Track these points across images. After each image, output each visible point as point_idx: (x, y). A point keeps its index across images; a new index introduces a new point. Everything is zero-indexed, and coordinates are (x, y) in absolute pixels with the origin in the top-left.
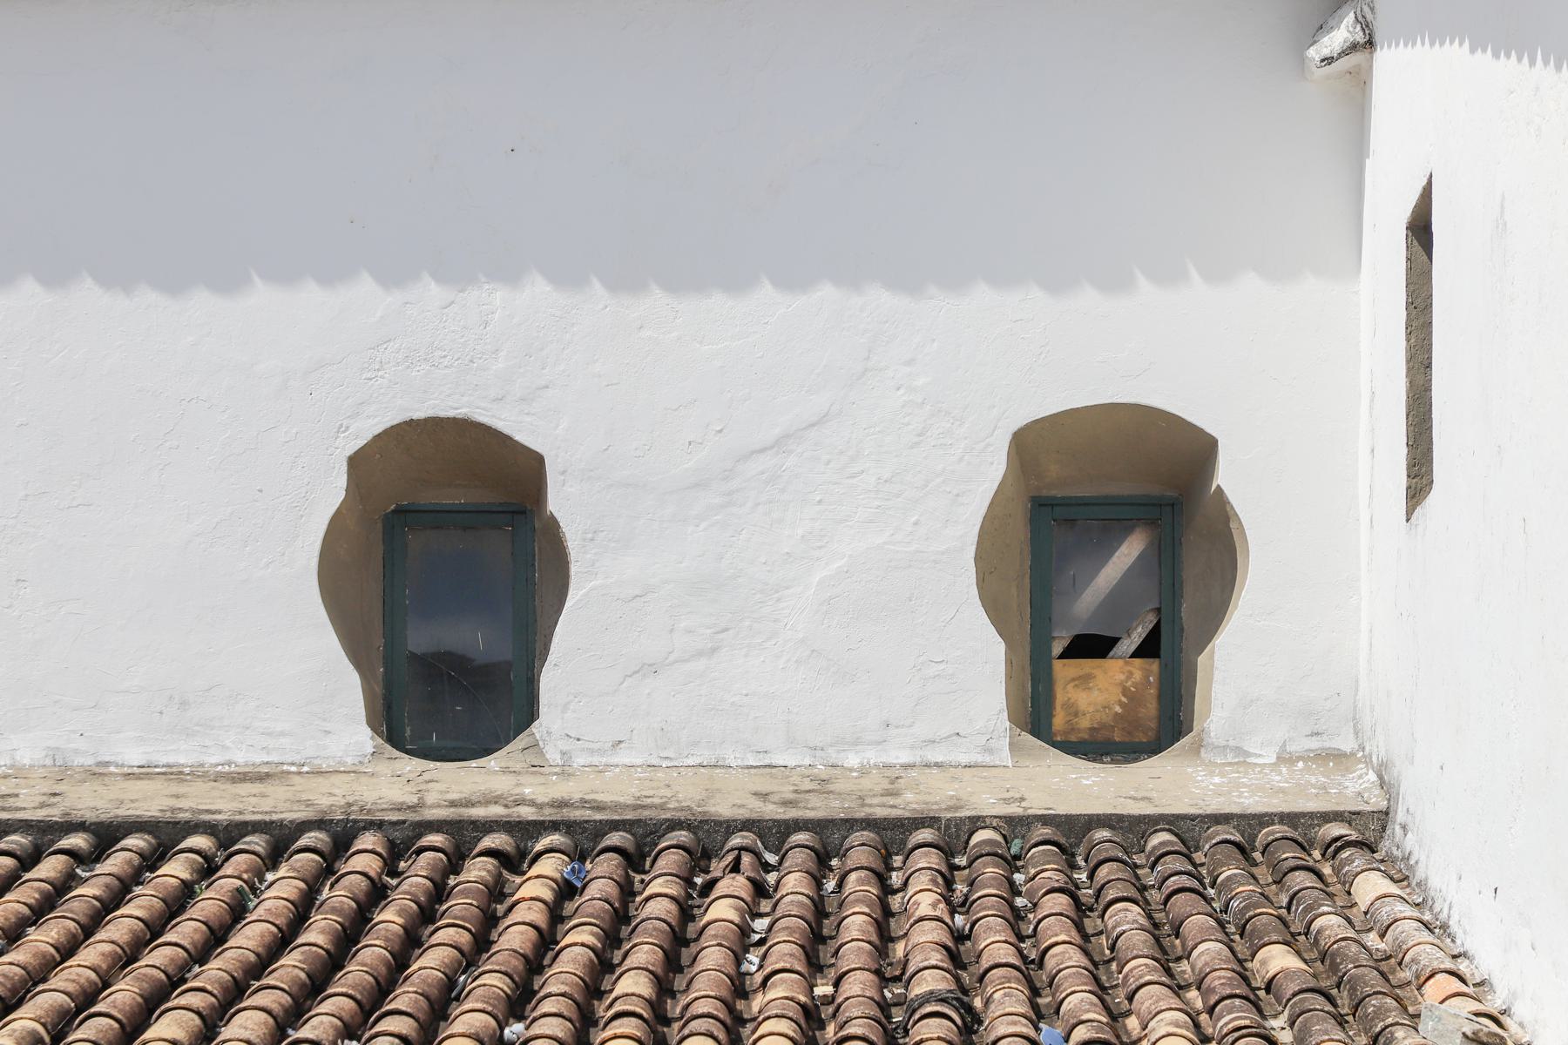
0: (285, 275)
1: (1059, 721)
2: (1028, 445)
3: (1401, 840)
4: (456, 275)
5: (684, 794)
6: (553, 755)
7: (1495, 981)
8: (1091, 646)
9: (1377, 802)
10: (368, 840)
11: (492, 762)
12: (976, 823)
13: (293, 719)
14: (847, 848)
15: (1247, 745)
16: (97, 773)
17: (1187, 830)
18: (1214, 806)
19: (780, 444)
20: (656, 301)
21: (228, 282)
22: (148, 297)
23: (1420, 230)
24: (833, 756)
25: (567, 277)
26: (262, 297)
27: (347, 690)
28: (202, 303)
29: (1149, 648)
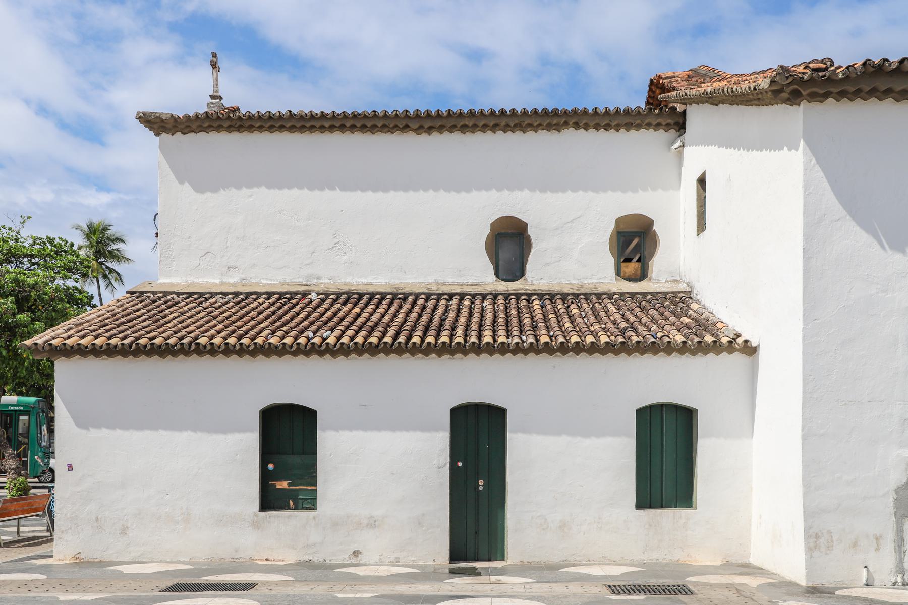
0: (479, 189)
1: (622, 274)
2: (619, 221)
3: (693, 295)
4: (511, 189)
5: (557, 289)
6: (529, 281)
8: (628, 260)
9: (688, 289)
10: (500, 297)
11: (518, 282)
12: (615, 294)
13: (480, 274)
14: (594, 297)
15: (658, 280)
16: (444, 284)
17: (644, 295)
18: (658, 290)
19: (572, 221)
20: (549, 194)
21: (468, 190)
22: (453, 193)
23: (702, 182)
25: (532, 189)
26: (475, 193)
27: (491, 268)
28: (463, 194)
29: (639, 260)
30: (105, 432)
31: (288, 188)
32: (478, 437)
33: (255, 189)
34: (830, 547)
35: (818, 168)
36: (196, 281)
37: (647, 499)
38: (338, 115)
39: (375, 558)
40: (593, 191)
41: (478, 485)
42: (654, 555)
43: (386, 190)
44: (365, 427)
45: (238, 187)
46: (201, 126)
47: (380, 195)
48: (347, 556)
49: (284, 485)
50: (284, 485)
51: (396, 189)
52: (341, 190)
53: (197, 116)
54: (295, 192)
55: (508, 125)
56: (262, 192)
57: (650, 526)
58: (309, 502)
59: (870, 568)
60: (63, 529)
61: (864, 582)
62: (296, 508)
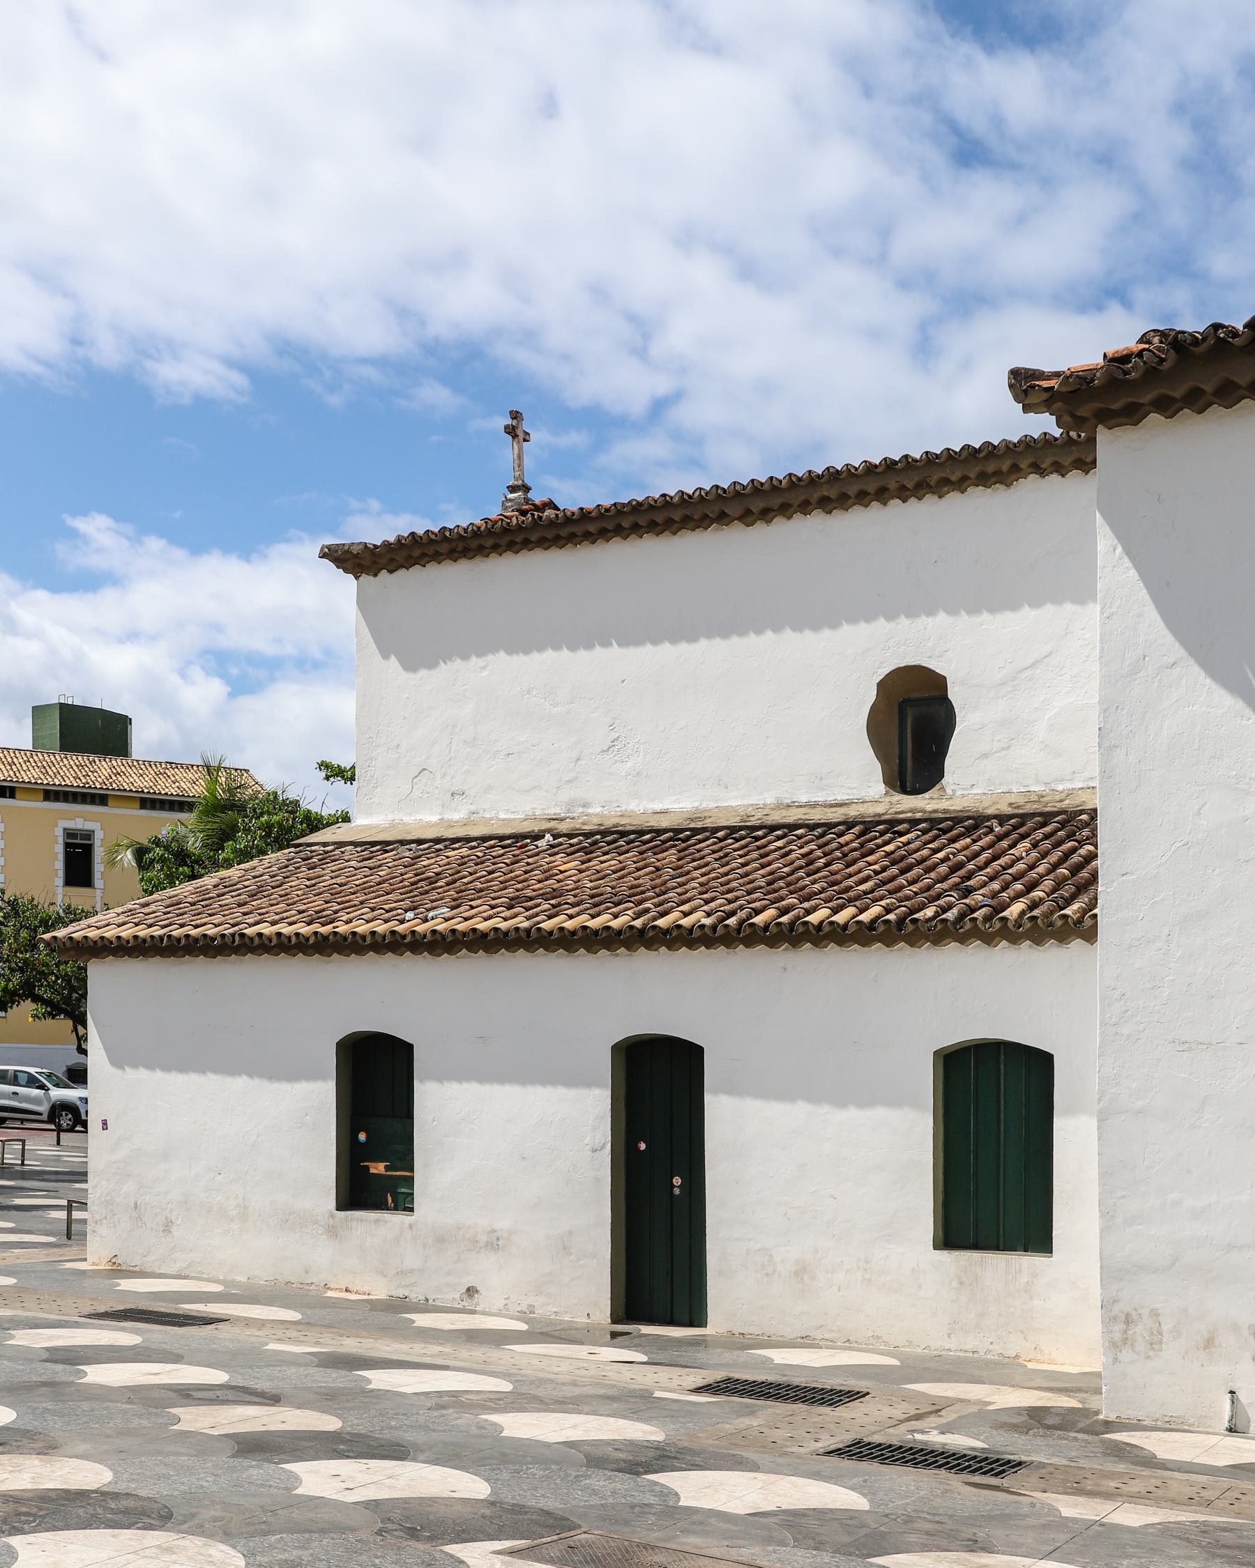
0: (853, 620)
4: (912, 614)
6: (949, 792)
7: (90, 1177)
11: (927, 795)
13: (855, 780)
19: (1033, 665)
20: (986, 616)
21: (834, 625)
24: (1053, 786)
25: (952, 611)
26: (846, 628)
28: (826, 633)
30: (143, 1073)
31: (539, 651)
32: (659, 1093)
33: (490, 657)
34: (1155, 1343)
35: (1127, 563)
36: (407, 819)
37: (957, 1230)
38: (607, 510)
39: (498, 1304)
40: (1074, 602)
41: (673, 1186)
42: (971, 1343)
43: (692, 638)
44: (482, 1079)
45: (465, 657)
46: (410, 557)
47: (683, 647)
48: (457, 1296)
49: (378, 1168)
50: (378, 1168)
51: (710, 636)
52: (620, 645)
53: (399, 541)
54: (549, 654)
55: (903, 488)
56: (501, 662)
57: (961, 1283)
58: (404, 1203)
59: (1241, 1395)
60: (97, 1217)
61: (1227, 1425)
62: (396, 1209)
